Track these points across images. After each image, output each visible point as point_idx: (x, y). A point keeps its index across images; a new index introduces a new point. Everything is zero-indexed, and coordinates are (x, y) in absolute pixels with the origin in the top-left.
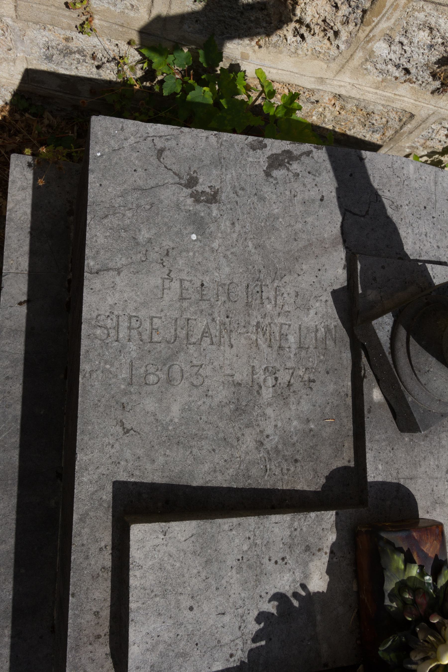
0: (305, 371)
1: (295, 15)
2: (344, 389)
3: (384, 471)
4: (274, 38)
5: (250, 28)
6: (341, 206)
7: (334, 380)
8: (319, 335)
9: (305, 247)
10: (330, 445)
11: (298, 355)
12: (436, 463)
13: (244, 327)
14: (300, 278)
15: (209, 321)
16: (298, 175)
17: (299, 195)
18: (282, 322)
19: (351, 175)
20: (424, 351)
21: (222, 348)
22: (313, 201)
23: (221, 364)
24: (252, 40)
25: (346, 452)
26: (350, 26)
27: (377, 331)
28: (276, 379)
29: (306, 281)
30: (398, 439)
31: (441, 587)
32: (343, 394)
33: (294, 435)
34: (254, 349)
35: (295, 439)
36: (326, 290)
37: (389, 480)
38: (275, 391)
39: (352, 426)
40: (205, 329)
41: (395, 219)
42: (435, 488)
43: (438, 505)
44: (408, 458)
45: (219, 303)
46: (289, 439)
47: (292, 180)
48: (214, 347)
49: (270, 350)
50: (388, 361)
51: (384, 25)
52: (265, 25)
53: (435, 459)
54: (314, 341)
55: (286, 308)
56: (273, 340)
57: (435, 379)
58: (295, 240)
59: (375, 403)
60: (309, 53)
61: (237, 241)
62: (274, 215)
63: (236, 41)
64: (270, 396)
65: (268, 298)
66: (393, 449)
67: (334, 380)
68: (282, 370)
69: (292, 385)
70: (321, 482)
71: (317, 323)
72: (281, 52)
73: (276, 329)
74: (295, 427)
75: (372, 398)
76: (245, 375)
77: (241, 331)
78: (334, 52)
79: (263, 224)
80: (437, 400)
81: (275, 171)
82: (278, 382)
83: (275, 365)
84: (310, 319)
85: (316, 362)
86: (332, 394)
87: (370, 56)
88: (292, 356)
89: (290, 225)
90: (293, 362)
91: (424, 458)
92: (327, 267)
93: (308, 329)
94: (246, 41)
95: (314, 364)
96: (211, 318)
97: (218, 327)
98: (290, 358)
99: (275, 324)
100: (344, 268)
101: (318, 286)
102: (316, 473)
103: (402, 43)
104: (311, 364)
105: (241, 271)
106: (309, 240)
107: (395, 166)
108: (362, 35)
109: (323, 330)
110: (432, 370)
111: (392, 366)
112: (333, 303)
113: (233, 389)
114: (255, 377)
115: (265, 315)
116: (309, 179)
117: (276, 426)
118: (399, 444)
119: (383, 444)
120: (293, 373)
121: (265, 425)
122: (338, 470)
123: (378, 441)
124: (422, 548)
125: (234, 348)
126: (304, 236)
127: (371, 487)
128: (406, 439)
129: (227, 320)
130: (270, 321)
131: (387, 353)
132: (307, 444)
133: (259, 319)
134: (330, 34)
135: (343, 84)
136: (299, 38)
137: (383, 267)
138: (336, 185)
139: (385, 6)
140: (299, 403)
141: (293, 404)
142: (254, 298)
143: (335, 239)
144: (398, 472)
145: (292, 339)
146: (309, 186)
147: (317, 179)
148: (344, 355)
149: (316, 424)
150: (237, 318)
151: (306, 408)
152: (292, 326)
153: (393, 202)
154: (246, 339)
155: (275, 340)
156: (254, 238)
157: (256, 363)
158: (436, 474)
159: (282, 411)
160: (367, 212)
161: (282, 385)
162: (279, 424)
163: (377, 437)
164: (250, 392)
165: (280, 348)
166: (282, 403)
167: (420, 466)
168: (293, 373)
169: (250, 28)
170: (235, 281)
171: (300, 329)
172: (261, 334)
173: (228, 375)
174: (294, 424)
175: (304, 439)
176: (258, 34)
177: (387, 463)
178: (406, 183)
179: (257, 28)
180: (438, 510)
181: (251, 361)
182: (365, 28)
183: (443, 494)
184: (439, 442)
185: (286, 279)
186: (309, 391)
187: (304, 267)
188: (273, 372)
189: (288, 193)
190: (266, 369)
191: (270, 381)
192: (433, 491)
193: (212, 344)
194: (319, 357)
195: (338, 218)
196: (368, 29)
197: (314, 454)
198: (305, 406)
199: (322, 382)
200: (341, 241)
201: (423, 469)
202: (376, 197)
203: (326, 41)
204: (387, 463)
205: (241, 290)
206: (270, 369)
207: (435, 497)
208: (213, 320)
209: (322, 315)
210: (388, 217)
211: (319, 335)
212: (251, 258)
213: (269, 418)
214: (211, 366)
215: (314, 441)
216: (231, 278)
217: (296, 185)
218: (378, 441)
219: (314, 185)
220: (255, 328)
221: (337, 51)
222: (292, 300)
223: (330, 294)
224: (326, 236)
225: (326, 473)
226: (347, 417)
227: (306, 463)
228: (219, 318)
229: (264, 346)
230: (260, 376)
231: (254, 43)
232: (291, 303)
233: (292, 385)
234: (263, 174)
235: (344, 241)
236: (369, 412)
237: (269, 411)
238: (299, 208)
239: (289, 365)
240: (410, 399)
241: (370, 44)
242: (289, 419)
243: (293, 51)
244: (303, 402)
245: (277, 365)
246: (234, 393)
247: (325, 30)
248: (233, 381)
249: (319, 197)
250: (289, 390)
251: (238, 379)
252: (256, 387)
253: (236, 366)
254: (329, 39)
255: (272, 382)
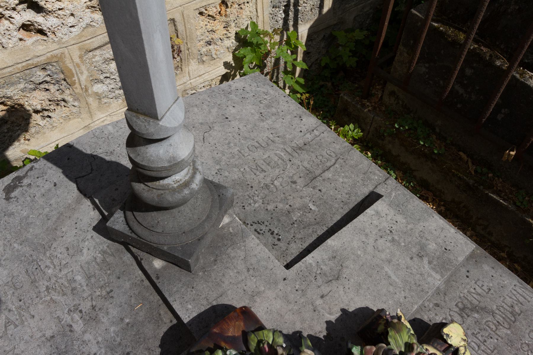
0: (101, 290)
1: (28, 111)
2: (137, 279)
3: (195, 307)
4: (32, 130)
5: (11, 136)
6: (71, 179)
7: (127, 278)
8: (98, 260)
9: (58, 218)
10: (149, 322)
11: (89, 284)
12: (235, 271)
13: (37, 297)
14: (64, 238)
15: (6, 314)
16: (30, 184)
17: (37, 194)
18: (66, 273)
19: (68, 159)
20: (147, 213)
21: (26, 323)
22: (49, 190)
23: (30, 334)
24: (19, 140)
25: (164, 317)
26: (66, 92)
27: (113, 227)
28: (81, 311)
29: (70, 238)
30: (193, 278)
31: (255, 350)
32: (139, 282)
33: (116, 336)
34: (52, 305)
35: (118, 339)
36: (88, 231)
37: (203, 310)
38: (85, 320)
39: (158, 297)
40: (5, 322)
41: (113, 159)
42: (245, 288)
43: (256, 297)
44: (210, 284)
45: (9, 297)
46: (114, 343)
47: (28, 190)
48: (19, 328)
49: (65, 297)
50: (135, 238)
51: (84, 78)
52: (18, 128)
53: (233, 270)
54: (97, 267)
55: (64, 262)
56: (64, 289)
57: (166, 223)
58: (49, 219)
59: (159, 269)
60: (62, 121)
61: (4, 250)
62: (25, 217)
63: (11, 148)
64: (82, 325)
65: (46, 267)
66: (193, 288)
67: (127, 278)
68: (82, 302)
69: (95, 306)
70: (157, 353)
71: (92, 255)
72: (44, 133)
73: (63, 281)
74: (114, 331)
75: (156, 268)
76: (54, 327)
77: (37, 302)
78: (74, 110)
79: (19, 228)
80: (182, 234)
81: (12, 194)
82: (83, 312)
83: (75, 303)
84: (86, 256)
85: (106, 278)
86: (130, 289)
87: (99, 96)
88: (85, 288)
89: (40, 214)
90: (88, 291)
91: (224, 275)
92: (81, 218)
93: (88, 263)
94: (16, 144)
95: (105, 281)
96: (7, 311)
97: (16, 313)
98: (84, 290)
99: (61, 278)
100: (94, 209)
101: (81, 232)
102: (149, 349)
103: (106, 77)
104: (102, 282)
105: (17, 265)
106: (58, 213)
107: (96, 135)
108: (78, 91)
109: (100, 255)
110: (159, 220)
111: (139, 238)
112: (97, 235)
113: (49, 344)
114: (62, 323)
115: (50, 278)
116: (40, 181)
117: (98, 343)
118: (196, 281)
119: (182, 291)
120: (92, 298)
121: (88, 349)
122: (166, 333)
123: (177, 291)
124: (226, 335)
125: (36, 316)
126: (54, 213)
127: (190, 325)
128: (200, 274)
129: (21, 303)
130: (55, 279)
131: (130, 234)
132: (130, 336)
133: (46, 283)
134: (63, 103)
135: (102, 119)
136: (48, 119)
137: (117, 189)
138: (61, 171)
139: (71, 70)
140: (107, 313)
141: (104, 317)
142: (35, 274)
143: (78, 199)
144: (207, 299)
145: (78, 278)
146: (42, 185)
147: (45, 177)
148: (125, 258)
149: (130, 317)
150: (28, 296)
151: (115, 313)
152: (74, 270)
153: (107, 152)
154: (42, 304)
155: (66, 287)
156: (17, 240)
157: (59, 313)
158: (240, 278)
159: (97, 329)
160: (92, 170)
161: (87, 312)
162: (100, 339)
163: (175, 289)
164: (64, 335)
165: (73, 289)
166: (94, 323)
167: (223, 282)
168: (92, 298)
169: (11, 136)
170: (15, 274)
171: (82, 267)
172: (53, 292)
173: (41, 337)
174: (112, 330)
175: (126, 335)
176: (19, 136)
177: (194, 300)
178: (110, 137)
179: (15, 133)
180: (258, 300)
181: (54, 315)
182: (75, 86)
183: (255, 286)
184: (229, 257)
185: (55, 245)
186: (111, 300)
187: (64, 230)
188: (76, 309)
189: (28, 198)
190: (70, 311)
191: (77, 316)
192: (245, 291)
193: (16, 326)
194: (106, 273)
195: (73, 186)
196: (77, 85)
197: (140, 338)
198: (114, 312)
199: (118, 287)
200: (83, 196)
201: (227, 283)
202: (94, 157)
203: (64, 108)
204: (194, 300)
205: (22, 277)
206: (72, 309)
207: (250, 293)
208: (10, 311)
209: (94, 246)
210: (108, 162)
211: (98, 260)
212: (21, 253)
213: (89, 341)
214: (23, 342)
215: (135, 329)
216: (11, 275)
217: (32, 191)
218: (177, 291)
219: (45, 182)
220: (46, 292)
221: (76, 108)
222: (66, 255)
223: (92, 231)
224: (70, 202)
225: (158, 343)
226: (151, 294)
227: (137, 350)
228: (14, 306)
229: (59, 298)
230: (67, 319)
231: (22, 141)
232: (66, 257)
233: (95, 306)
234: (4, 201)
235: (85, 195)
236: (158, 278)
237: (87, 337)
238: (41, 201)
239: (85, 295)
240: (165, 248)
241: (90, 91)
242: (106, 330)
243: (51, 127)
244: (111, 310)
245: (77, 302)
246: (51, 346)
247: (58, 105)
248: (46, 339)
249: (53, 185)
250: (95, 310)
251: (49, 334)
252: (67, 329)
253: (43, 327)
254: (65, 106)
255: (79, 316)
